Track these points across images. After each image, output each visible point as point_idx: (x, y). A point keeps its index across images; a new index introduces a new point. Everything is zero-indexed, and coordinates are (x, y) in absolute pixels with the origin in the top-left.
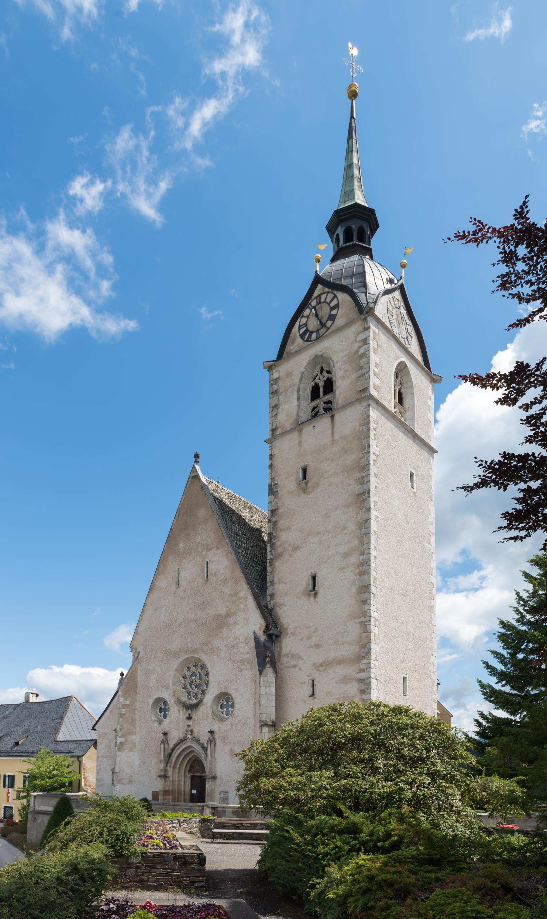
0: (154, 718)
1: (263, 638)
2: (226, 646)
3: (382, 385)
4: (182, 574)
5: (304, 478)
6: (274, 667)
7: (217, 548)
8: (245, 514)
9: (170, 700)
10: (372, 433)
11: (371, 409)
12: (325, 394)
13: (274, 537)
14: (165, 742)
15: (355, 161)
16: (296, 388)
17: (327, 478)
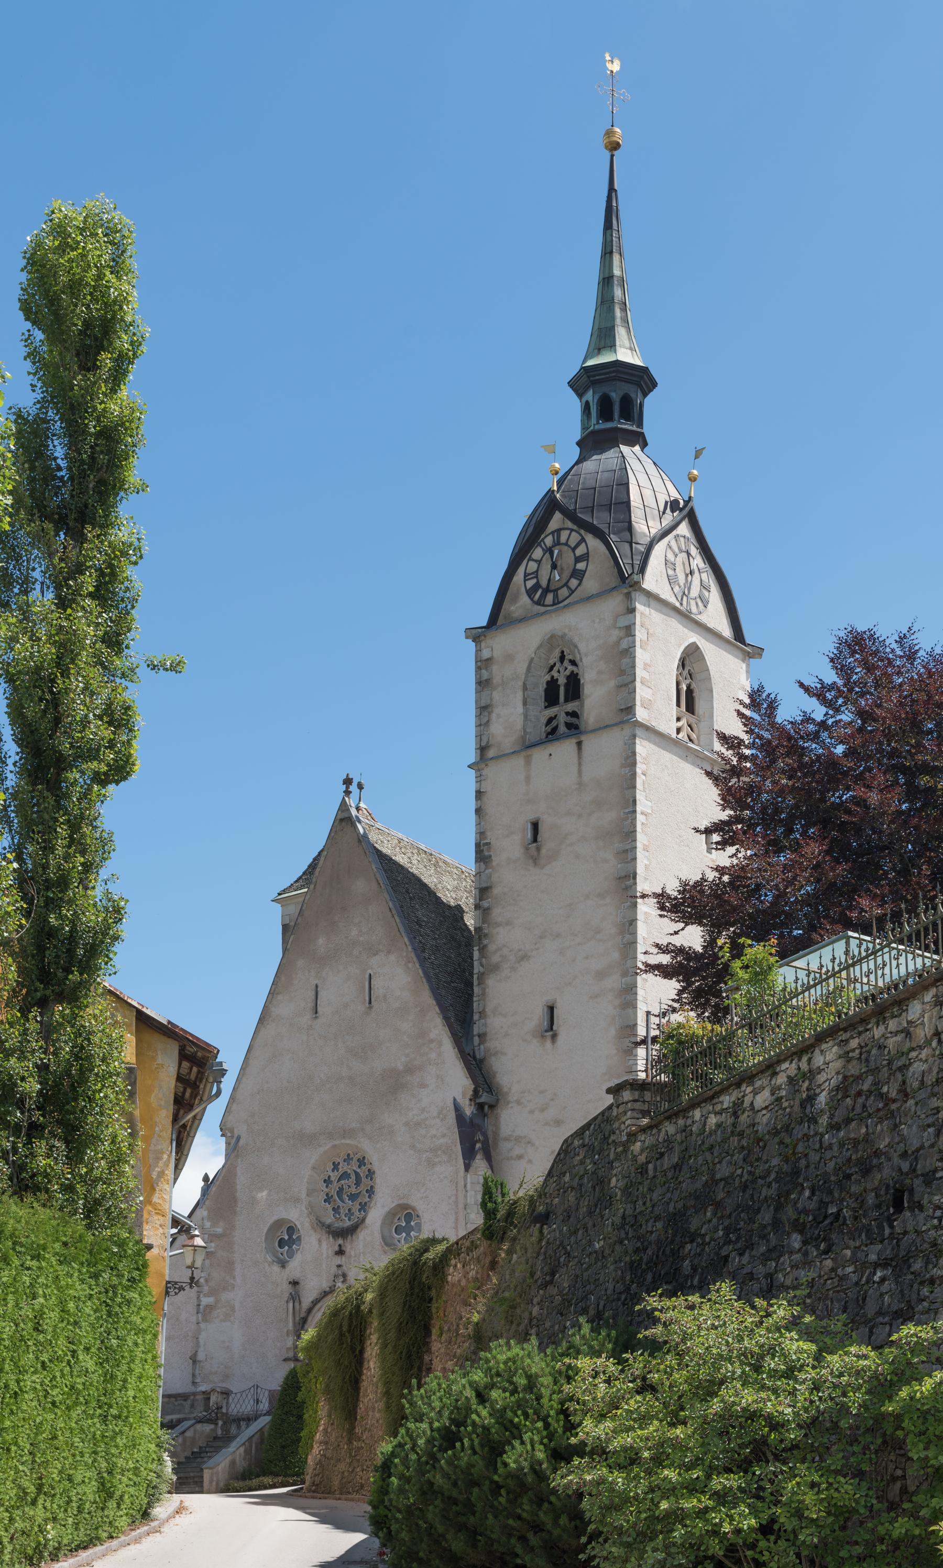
1: (469, 1110)
2: (407, 1124)
3: (656, 701)
5: (535, 840)
6: (488, 1158)
7: (389, 952)
8: (429, 878)
9: (303, 1224)
11: (638, 741)
13: (486, 935)
14: (295, 1297)
15: (617, 272)
16: (520, 683)
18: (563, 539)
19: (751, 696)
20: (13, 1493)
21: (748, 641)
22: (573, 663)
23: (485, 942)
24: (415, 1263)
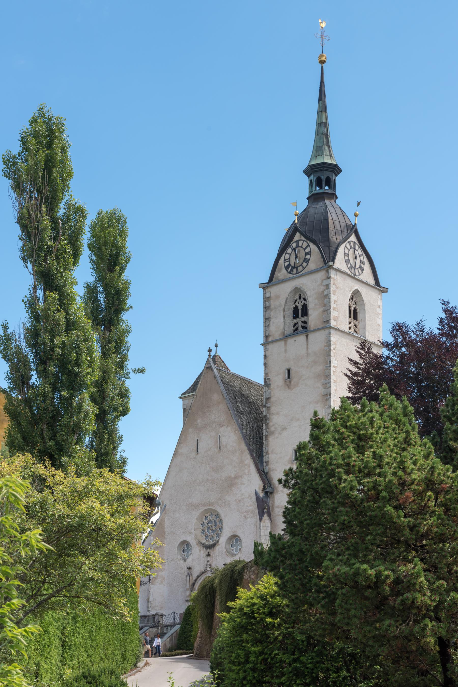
0: (179, 557)
1: (261, 495)
2: (236, 500)
3: (340, 317)
4: (200, 444)
5: (289, 378)
6: (269, 515)
10: (332, 354)
12: (302, 316)
13: (268, 419)
16: (282, 308)
17: (304, 380)
18: (300, 245)
19: (361, 345)
20: (99, 659)
21: (381, 285)
22: (305, 299)
23: (268, 422)
24: (232, 571)
